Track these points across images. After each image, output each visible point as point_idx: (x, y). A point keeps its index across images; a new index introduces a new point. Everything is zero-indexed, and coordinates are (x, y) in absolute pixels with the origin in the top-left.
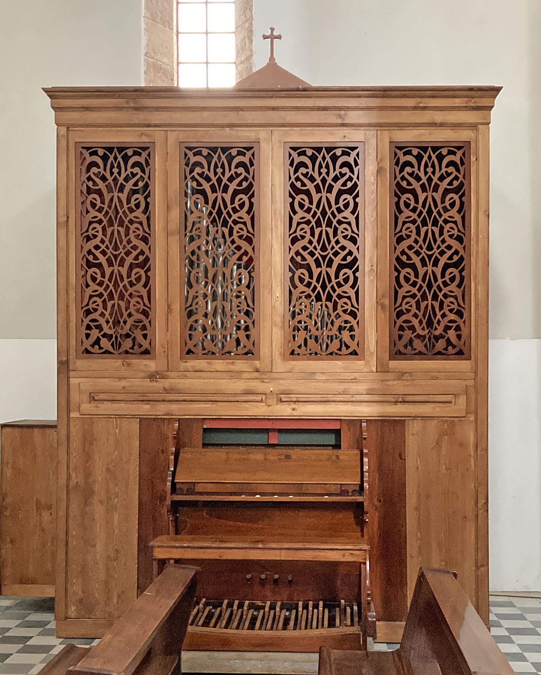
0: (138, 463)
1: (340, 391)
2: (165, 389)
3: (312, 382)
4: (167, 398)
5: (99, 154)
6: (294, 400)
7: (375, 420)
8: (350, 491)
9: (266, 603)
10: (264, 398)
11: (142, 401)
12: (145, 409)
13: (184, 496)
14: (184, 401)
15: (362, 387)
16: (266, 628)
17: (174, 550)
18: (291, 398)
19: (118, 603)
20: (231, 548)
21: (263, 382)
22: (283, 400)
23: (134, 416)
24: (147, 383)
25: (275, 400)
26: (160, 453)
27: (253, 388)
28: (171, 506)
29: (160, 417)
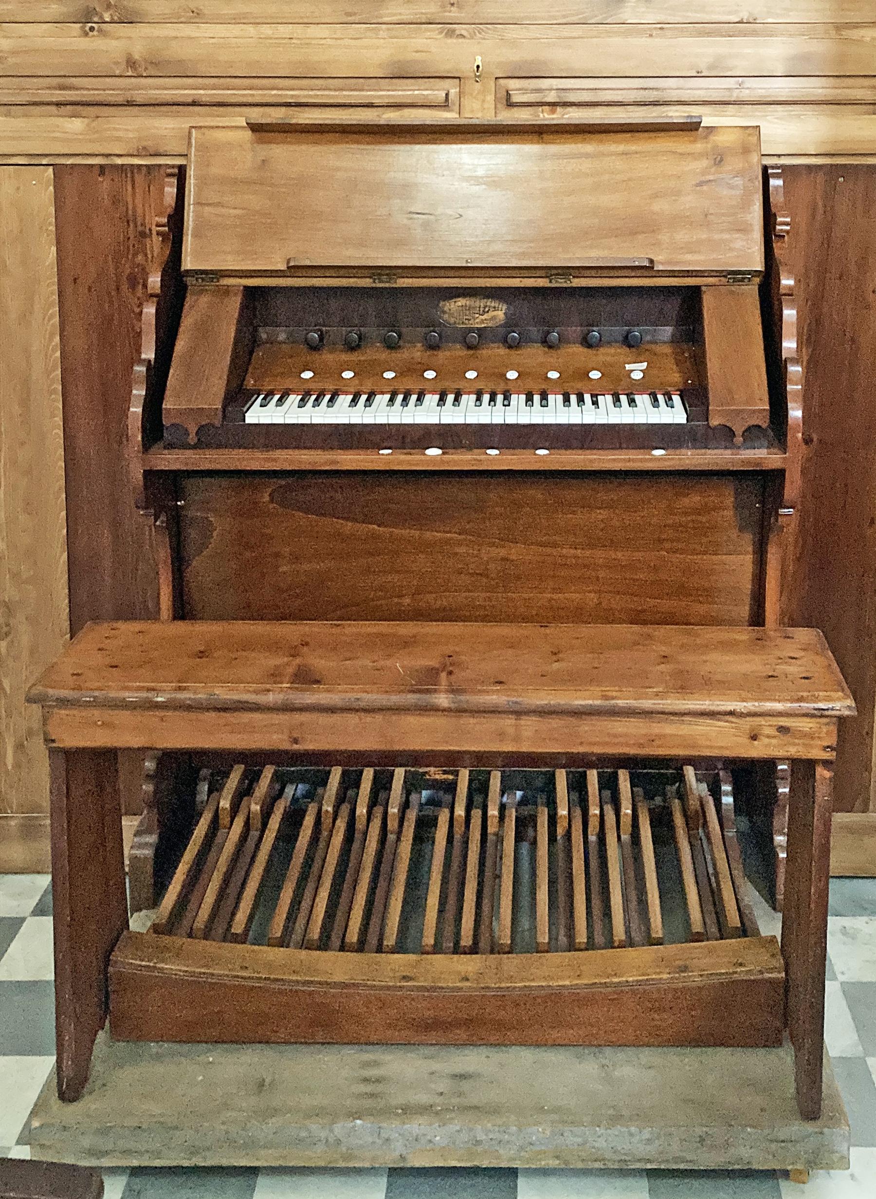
0: (57, 319)
1: (703, 66)
2: (131, 63)
3: (609, 34)
4: (139, 96)
5: (533, 337)
6: (551, 97)
7: (809, 168)
8: (739, 430)
9: (456, 774)
10: (453, 92)
11: (58, 104)
12: (70, 135)
13: (189, 453)
14: (194, 104)
15: (775, 52)
16: (457, 943)
17: (123, 717)
18: (538, 90)
19: (17, 765)
20: (331, 710)
21: (450, 34)
22: (516, 99)
23: (34, 161)
24: (72, 39)
25: (490, 98)
26: (125, 287)
27: (418, 56)
28: (146, 487)
29: (119, 161)
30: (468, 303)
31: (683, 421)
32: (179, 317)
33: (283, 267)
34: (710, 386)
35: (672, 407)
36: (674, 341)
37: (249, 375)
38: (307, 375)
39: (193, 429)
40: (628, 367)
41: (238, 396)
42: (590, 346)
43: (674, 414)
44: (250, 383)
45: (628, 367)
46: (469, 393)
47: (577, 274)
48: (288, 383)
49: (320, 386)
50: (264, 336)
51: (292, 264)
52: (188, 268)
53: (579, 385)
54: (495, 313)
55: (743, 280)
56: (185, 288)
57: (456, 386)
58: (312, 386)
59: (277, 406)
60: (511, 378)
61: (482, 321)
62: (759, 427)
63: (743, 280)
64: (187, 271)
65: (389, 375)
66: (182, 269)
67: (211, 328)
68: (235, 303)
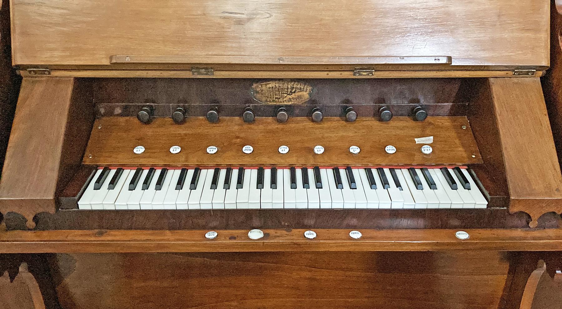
8: (535, 215)
30: (277, 85)
31: (485, 207)
32: (14, 108)
33: (106, 62)
34: (509, 179)
35: (469, 189)
36: (453, 113)
37: (88, 150)
38: (139, 150)
39: (30, 218)
40: (418, 141)
41: (74, 175)
42: (381, 120)
43: (473, 198)
44: (88, 160)
45: (418, 141)
46: (283, 168)
47: (378, 69)
48: (122, 159)
49: (151, 161)
50: (102, 111)
51: (114, 61)
52: (19, 63)
53: (379, 160)
54: (300, 93)
55: (527, 73)
56: (20, 78)
57: (272, 162)
58: (143, 161)
59: (109, 189)
60: (319, 153)
61: (290, 100)
62: (554, 213)
63: (527, 73)
64: (17, 66)
65: (212, 150)
66: (13, 64)
67: (41, 126)
68: (69, 90)
